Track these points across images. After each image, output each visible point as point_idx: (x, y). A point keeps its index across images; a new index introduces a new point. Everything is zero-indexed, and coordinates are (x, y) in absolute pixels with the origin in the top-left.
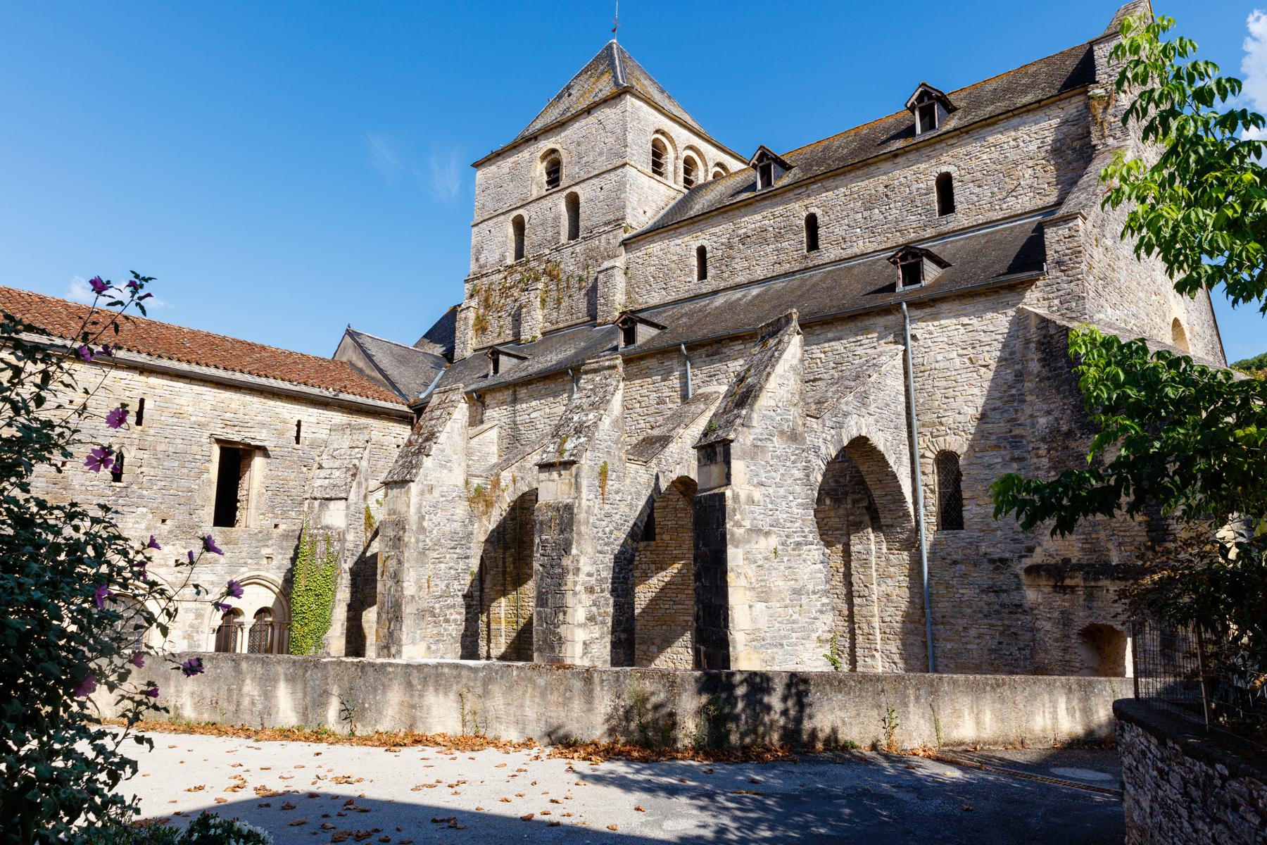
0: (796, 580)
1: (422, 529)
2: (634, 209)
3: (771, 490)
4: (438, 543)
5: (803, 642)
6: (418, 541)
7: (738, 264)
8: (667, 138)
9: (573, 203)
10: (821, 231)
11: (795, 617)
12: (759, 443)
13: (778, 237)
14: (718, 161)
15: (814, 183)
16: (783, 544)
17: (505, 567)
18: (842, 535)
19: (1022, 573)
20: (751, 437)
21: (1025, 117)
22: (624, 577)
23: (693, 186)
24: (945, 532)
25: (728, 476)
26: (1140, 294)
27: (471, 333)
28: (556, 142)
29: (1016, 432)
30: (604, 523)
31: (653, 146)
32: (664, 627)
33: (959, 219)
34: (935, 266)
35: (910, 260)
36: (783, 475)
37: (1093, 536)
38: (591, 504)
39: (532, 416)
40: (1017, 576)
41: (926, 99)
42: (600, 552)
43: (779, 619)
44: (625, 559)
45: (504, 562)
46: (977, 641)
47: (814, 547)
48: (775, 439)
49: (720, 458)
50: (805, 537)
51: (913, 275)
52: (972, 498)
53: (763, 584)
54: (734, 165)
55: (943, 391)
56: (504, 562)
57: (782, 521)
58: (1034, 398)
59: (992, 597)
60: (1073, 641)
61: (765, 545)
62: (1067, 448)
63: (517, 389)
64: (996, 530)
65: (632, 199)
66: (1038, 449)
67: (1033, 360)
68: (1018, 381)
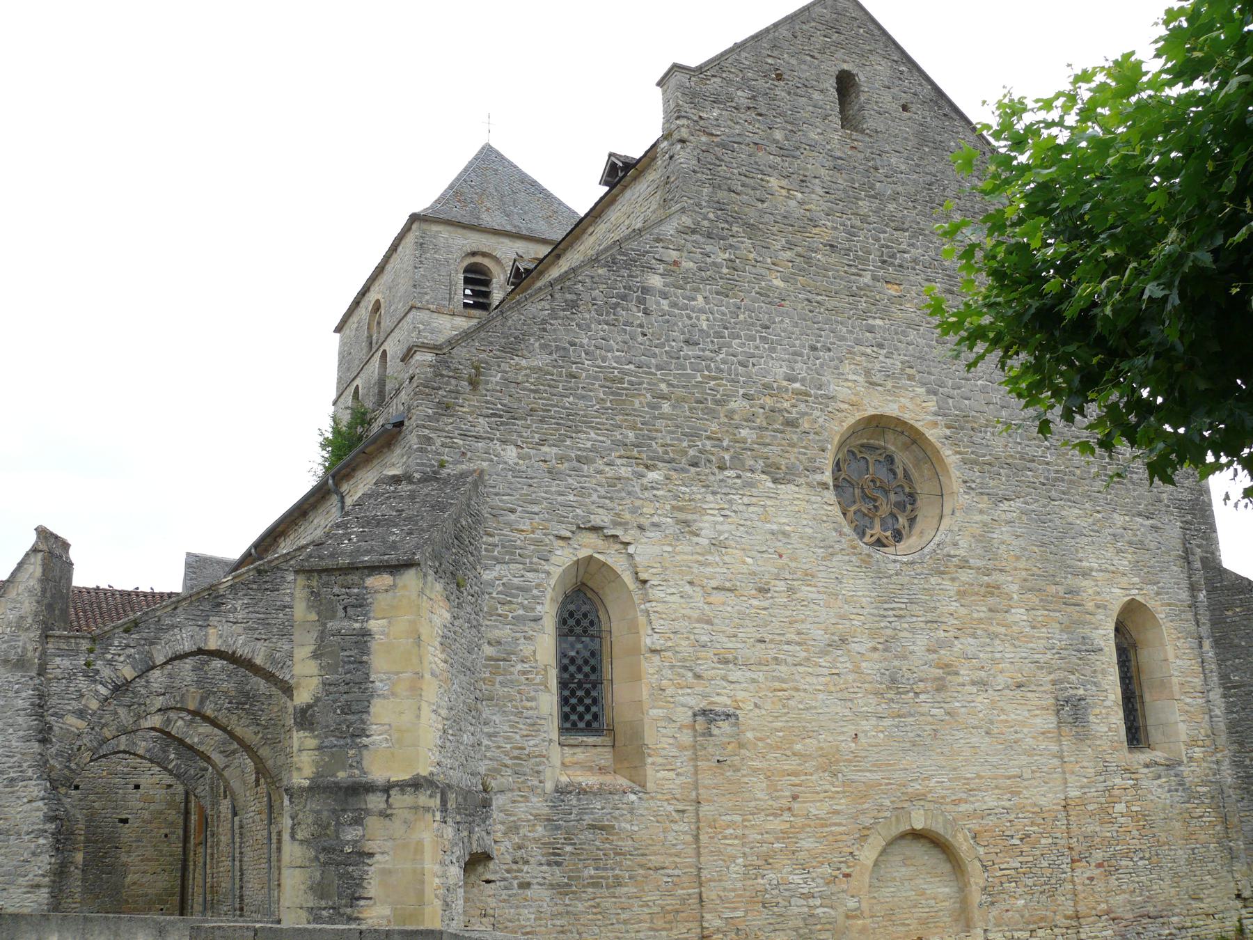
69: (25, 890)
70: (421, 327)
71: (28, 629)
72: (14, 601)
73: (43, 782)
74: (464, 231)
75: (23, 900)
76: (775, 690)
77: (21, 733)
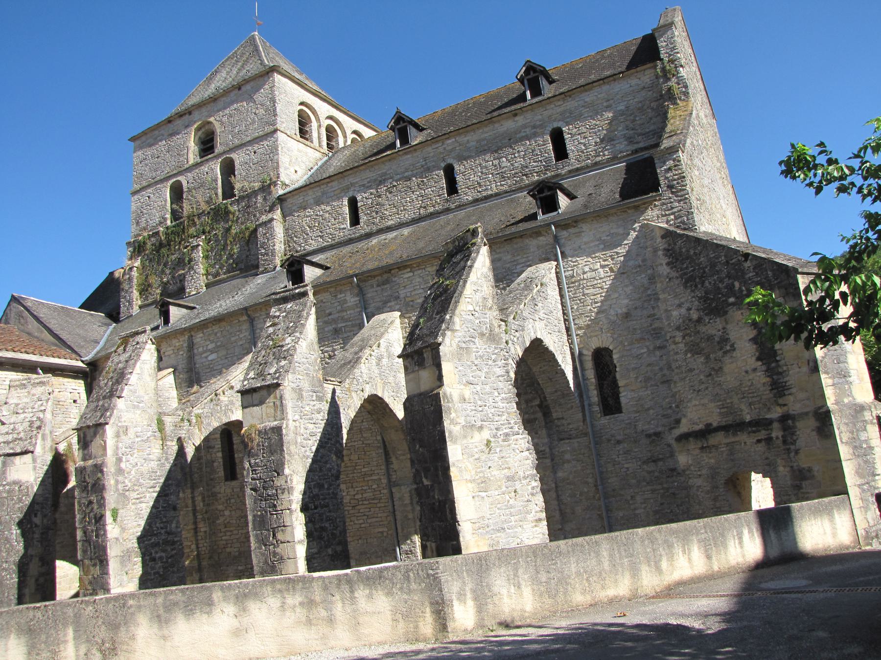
1: (120, 471)
2: (286, 169)
3: (478, 388)
4: (137, 483)
5: (521, 523)
6: (117, 482)
8: (311, 111)
9: (229, 169)
11: (512, 502)
16: (494, 437)
17: (194, 506)
19: (673, 442)
20: (457, 340)
22: (333, 493)
24: (608, 417)
25: (440, 377)
27: (136, 294)
29: (657, 325)
31: (299, 116)
34: (565, 198)
35: (547, 193)
37: (728, 401)
38: (298, 424)
39: (210, 358)
40: (669, 445)
41: (532, 73)
43: (499, 506)
44: (332, 475)
45: (194, 502)
46: (643, 506)
47: (520, 436)
48: (476, 340)
49: (429, 361)
50: (511, 428)
51: (550, 205)
52: (626, 385)
53: (481, 475)
54: (368, 133)
55: (592, 297)
56: (194, 502)
57: (490, 415)
58: (666, 295)
59: (651, 467)
60: (721, 490)
61: (479, 438)
62: (698, 332)
63: (193, 333)
64: (649, 409)
65: (284, 159)
66: (674, 337)
67: (661, 264)
71: (491, 308)
77: (503, 395)
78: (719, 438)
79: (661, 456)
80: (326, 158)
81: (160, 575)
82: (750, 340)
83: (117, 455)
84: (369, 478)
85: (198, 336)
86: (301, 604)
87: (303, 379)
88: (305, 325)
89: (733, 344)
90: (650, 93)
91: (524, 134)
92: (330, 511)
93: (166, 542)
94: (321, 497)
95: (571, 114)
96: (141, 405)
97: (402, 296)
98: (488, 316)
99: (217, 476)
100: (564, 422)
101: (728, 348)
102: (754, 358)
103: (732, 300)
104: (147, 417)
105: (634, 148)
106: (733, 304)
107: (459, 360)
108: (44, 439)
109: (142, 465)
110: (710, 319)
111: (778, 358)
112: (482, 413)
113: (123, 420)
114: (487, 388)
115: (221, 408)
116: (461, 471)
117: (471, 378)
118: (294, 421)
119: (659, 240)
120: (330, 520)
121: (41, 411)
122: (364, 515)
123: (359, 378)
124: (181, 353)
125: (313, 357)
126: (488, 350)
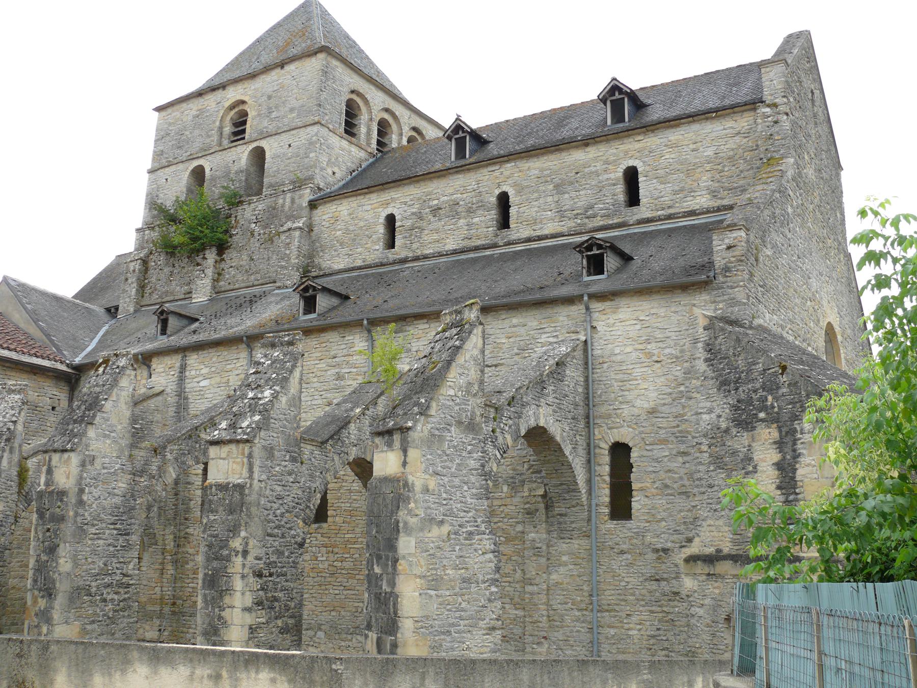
0: (467, 569)
1: (81, 503)
2: (322, 169)
4: (97, 518)
6: (77, 514)
7: (427, 237)
9: (259, 155)
10: (513, 211)
11: (464, 605)
12: (437, 432)
13: (470, 211)
14: (413, 125)
15: (508, 161)
18: (518, 523)
20: (429, 426)
21: (703, 124)
22: (294, 562)
23: (386, 150)
24: (615, 522)
26: (797, 300)
28: (245, 94)
29: (683, 427)
30: (275, 506)
31: (347, 106)
32: (333, 613)
33: (644, 211)
35: (595, 251)
36: (459, 465)
39: (202, 384)
41: (617, 93)
42: (269, 535)
43: (449, 607)
46: (639, 627)
50: (477, 526)
57: (455, 510)
59: (654, 586)
66: (700, 444)
68: (687, 379)
69: (484, 632)
70: (323, 141)
71: (475, 395)
72: (462, 367)
73: (494, 537)
74: (351, 72)
75: (483, 641)
76: (669, 471)
77: (474, 491)
78: (725, 567)
79: (665, 576)
80: (371, 160)
81: (109, 618)
82: (773, 464)
83: (80, 485)
84: (350, 546)
85: (192, 357)
86: (210, 677)
87: (278, 437)
88: (289, 378)
89: (756, 465)
90: (745, 140)
91: (593, 169)
92: (287, 581)
93: (121, 585)
94: (279, 564)
95: (650, 152)
96: (113, 434)
97: (414, 349)
98: (470, 403)
99: (192, 515)
100: (567, 519)
101: (751, 469)
102: (774, 486)
103: (762, 415)
104: (117, 448)
105: (716, 204)
106: (762, 420)
107: (429, 447)
108: (11, 451)
109: (105, 499)
110: (738, 432)
111: (797, 491)
112: (446, 507)
113: (91, 449)
114: (457, 481)
115: (200, 446)
116: (411, 565)
117: (439, 468)
118: (259, 481)
119: (701, 330)
120: (285, 590)
121: (12, 422)
122: (341, 585)
123: (346, 439)
124: (172, 373)
125: (292, 414)
126: (464, 440)
